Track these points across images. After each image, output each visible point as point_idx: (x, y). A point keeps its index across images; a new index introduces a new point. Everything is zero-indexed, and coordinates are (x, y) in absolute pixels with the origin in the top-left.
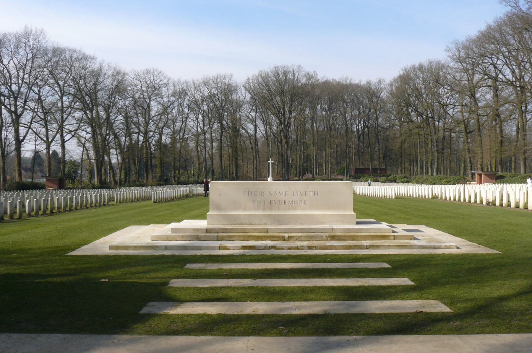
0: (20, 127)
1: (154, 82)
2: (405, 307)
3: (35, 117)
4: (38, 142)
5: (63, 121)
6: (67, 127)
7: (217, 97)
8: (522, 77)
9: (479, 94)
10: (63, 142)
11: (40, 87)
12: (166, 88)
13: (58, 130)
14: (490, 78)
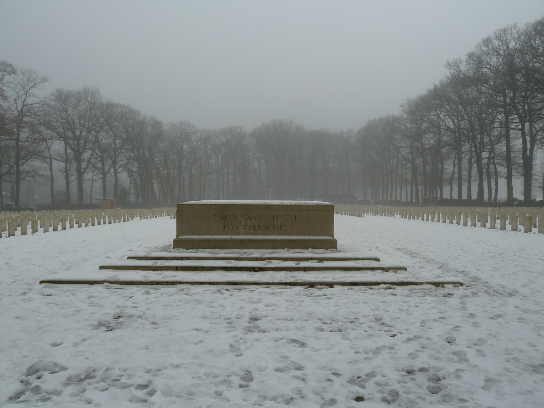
0: (444, 197)
1: (185, 131)
3: (93, 154)
4: (95, 173)
6: (120, 162)
8: (459, 125)
9: (425, 139)
10: (116, 173)
11: (97, 132)
12: (194, 136)
13: (112, 165)
14: (434, 126)
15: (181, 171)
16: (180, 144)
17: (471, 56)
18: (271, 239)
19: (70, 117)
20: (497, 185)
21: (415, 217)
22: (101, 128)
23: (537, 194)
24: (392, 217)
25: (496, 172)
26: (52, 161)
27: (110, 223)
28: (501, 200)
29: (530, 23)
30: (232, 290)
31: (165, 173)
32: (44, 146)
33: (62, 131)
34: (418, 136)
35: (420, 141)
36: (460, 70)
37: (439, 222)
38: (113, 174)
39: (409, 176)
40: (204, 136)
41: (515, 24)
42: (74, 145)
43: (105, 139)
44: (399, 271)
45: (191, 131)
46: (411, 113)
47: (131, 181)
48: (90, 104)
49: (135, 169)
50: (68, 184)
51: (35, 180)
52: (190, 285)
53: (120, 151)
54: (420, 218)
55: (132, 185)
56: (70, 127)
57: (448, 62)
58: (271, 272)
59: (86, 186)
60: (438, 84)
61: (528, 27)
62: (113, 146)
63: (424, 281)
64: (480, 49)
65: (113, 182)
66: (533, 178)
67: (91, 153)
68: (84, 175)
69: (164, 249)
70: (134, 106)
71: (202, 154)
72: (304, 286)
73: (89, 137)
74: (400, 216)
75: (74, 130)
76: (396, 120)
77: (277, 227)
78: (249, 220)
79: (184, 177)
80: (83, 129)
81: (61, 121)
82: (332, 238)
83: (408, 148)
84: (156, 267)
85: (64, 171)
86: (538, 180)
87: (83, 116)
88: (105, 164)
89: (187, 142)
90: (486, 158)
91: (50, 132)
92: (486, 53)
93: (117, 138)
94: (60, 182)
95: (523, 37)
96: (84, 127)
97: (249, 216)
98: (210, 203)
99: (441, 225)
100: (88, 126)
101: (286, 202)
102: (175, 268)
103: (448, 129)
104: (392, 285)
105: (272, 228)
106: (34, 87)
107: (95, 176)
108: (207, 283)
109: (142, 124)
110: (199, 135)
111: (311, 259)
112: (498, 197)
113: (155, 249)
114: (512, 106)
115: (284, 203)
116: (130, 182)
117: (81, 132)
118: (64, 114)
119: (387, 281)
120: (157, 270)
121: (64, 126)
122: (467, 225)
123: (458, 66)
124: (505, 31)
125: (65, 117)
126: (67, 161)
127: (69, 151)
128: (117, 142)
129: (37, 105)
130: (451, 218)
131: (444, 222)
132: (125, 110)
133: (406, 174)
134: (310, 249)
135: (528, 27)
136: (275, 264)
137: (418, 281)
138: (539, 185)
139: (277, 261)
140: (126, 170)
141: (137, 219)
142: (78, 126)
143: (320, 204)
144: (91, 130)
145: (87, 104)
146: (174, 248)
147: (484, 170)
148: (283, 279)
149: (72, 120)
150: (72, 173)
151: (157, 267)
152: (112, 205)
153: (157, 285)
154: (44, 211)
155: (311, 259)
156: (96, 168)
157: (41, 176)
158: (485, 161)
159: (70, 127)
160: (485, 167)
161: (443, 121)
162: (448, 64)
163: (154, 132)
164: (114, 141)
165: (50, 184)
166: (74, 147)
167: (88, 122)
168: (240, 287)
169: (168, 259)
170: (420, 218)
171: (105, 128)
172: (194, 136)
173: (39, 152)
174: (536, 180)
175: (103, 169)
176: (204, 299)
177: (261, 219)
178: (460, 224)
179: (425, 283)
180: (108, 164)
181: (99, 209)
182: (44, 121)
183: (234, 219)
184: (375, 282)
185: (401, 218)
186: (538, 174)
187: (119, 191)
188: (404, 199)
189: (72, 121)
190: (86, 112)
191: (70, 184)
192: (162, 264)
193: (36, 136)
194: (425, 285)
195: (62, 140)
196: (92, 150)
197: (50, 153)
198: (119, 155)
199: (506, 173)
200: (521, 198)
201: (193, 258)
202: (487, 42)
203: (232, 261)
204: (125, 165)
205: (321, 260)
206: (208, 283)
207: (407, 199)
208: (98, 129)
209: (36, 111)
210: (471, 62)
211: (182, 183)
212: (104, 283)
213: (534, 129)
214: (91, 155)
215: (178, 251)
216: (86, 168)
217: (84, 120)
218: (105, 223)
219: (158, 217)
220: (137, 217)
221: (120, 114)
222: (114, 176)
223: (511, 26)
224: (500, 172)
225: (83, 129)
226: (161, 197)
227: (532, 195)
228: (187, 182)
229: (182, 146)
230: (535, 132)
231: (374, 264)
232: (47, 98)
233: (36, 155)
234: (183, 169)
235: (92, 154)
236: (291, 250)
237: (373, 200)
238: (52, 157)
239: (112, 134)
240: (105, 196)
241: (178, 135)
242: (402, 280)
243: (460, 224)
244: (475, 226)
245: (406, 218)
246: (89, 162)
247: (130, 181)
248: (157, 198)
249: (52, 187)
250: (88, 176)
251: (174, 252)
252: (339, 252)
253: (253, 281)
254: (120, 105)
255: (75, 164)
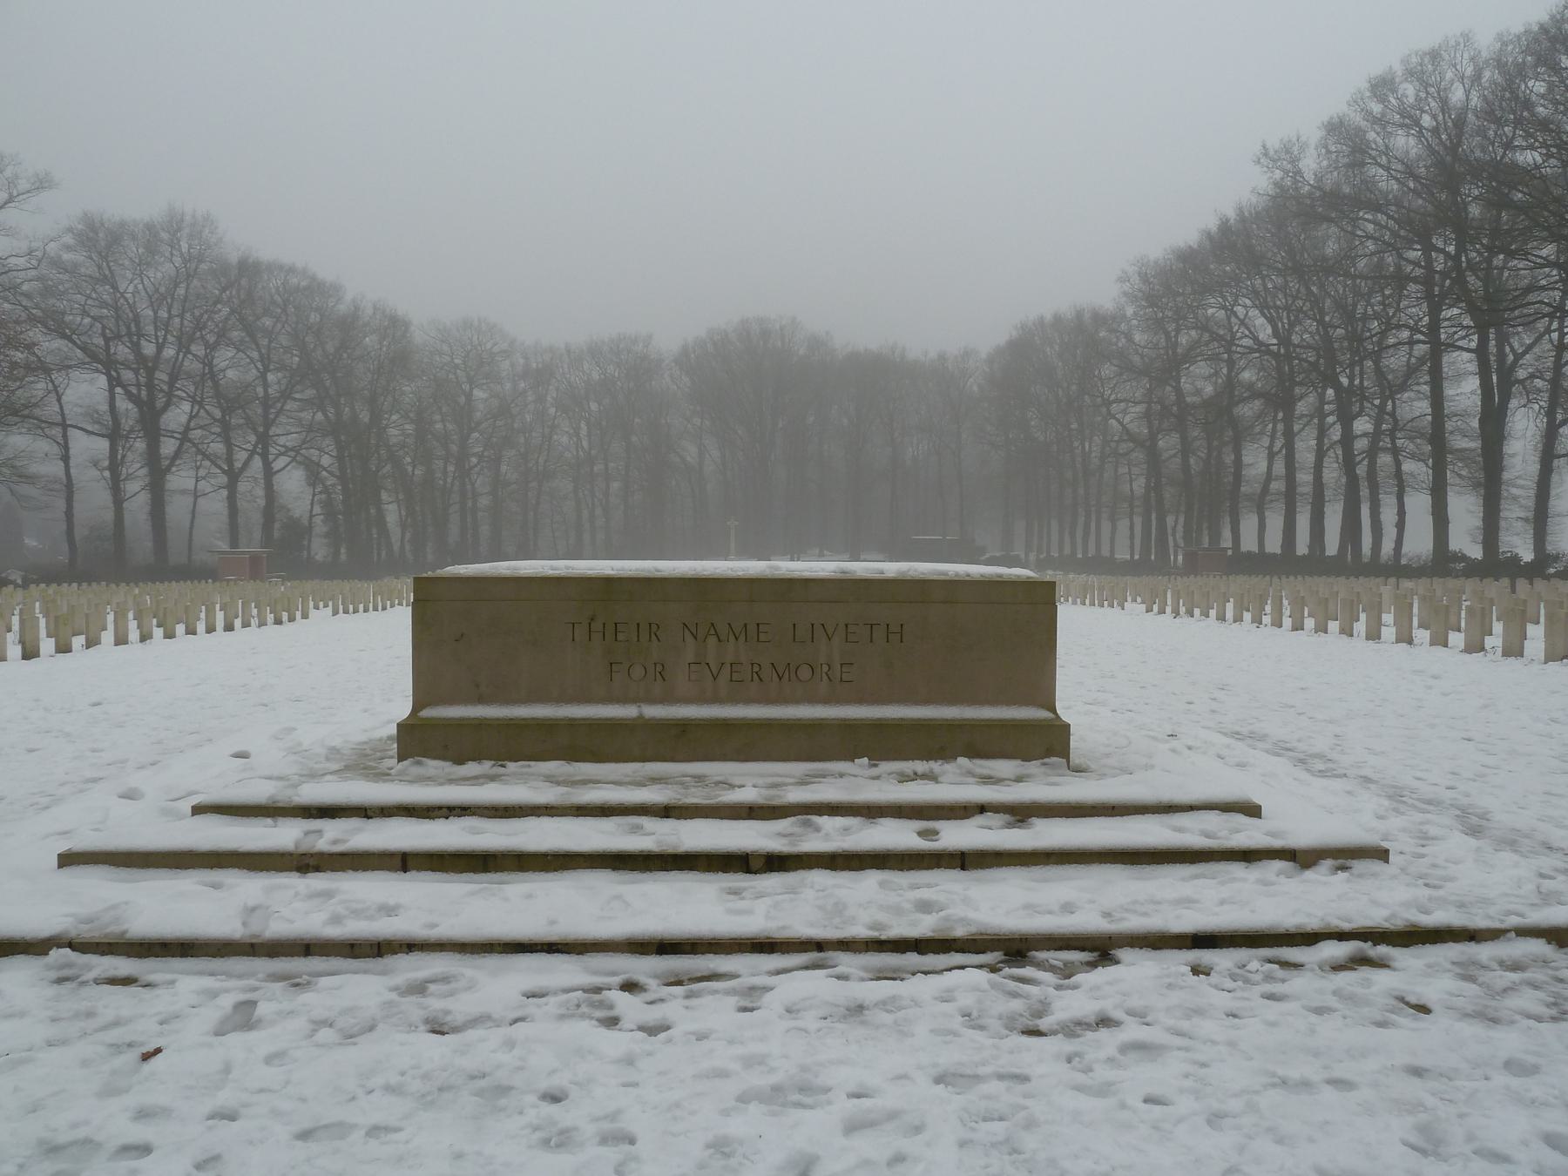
2: (823, 570)
4: (202, 472)
5: (268, 424)
6: (282, 440)
7: (618, 383)
10: (269, 473)
11: (211, 348)
12: (507, 362)
13: (255, 446)
15: (467, 467)
16: (463, 386)
17: (1336, 128)
18: (800, 720)
19: (126, 300)
20: (1401, 513)
21: (1195, 609)
22: (222, 335)
23: (1516, 540)
24: (1117, 609)
25: (1399, 474)
26: (68, 434)
27: (229, 627)
28: (1417, 556)
29: (1510, 34)
30: (655, 989)
31: (420, 472)
32: (40, 387)
33: (101, 342)
34: (1171, 365)
35: (1174, 384)
36: (1299, 172)
37: (1280, 626)
38: (260, 476)
39: (1139, 486)
40: (534, 365)
41: (1467, 35)
42: (138, 385)
43: (233, 367)
44: (1359, 866)
45: (495, 349)
46: (1152, 300)
47: (314, 495)
48: (185, 261)
49: (326, 461)
50: (118, 500)
51: (11, 491)
52: (458, 956)
53: (279, 405)
54: (1213, 613)
55: (317, 509)
56: (123, 331)
57: (1264, 147)
58: (819, 878)
59: (176, 510)
60: (1232, 214)
61: (1505, 44)
62: (260, 390)
63: (1502, 921)
64: (1362, 110)
65: (258, 500)
66: (1505, 494)
67: (189, 411)
68: (168, 477)
69: (362, 763)
70: (325, 272)
71: (528, 418)
72: (983, 952)
73: (183, 361)
74: (1143, 607)
75: (139, 339)
76: (1099, 319)
77: (825, 668)
78: (712, 640)
79: (476, 485)
80: (165, 338)
81: (94, 312)
82: (1043, 714)
83: (1136, 403)
84: (312, 855)
85: (106, 463)
86: (1521, 499)
87: (165, 298)
88: (237, 446)
89: (485, 381)
90: (1365, 435)
91: (59, 343)
92: (1380, 121)
93: (272, 367)
94: (94, 499)
95: (1487, 74)
96: (167, 331)
97: (713, 624)
98: (551, 572)
99: (1307, 638)
100: (181, 329)
101: (862, 568)
102: (398, 862)
103: (1261, 347)
104: (1370, 943)
105: (805, 673)
106: (10, 205)
107: (203, 482)
108: (536, 944)
109: (349, 325)
110: (522, 361)
111: (982, 809)
112: (1405, 549)
113: (328, 759)
114: (1450, 278)
115: (855, 571)
116: (313, 500)
117: (160, 348)
118: (105, 291)
119: (1346, 926)
120: (317, 869)
121: (104, 328)
122: (1379, 638)
123: (1294, 161)
124: (1434, 55)
125: (110, 301)
126: (114, 435)
127: (123, 404)
128: (271, 377)
129: (21, 262)
130: (1252, 607)
131: (1298, 626)
132: (294, 281)
133: (1131, 481)
134: (959, 759)
135: (1505, 44)
136: (833, 835)
137: (1479, 922)
138: (1522, 515)
139: (839, 821)
140: (300, 463)
141: (321, 618)
142: (150, 329)
143: (1001, 576)
144: (192, 340)
145: (178, 261)
146: (401, 758)
147: (1361, 470)
148: (882, 917)
149: (132, 307)
150: (130, 471)
151: (316, 854)
152: (256, 569)
153: (302, 960)
154: (70, 585)
155: (982, 809)
156: (206, 456)
157: (30, 479)
158: (1361, 444)
159: (123, 331)
160: (1363, 459)
161: (1242, 323)
162: (1266, 154)
163: (384, 349)
164: (263, 376)
165: (61, 504)
166: (139, 390)
167: (181, 316)
168: (691, 961)
169: (369, 813)
170: (1213, 613)
171: (235, 335)
172: (507, 362)
173: (26, 407)
174: (1515, 498)
175: (230, 460)
176: (520, 1068)
177: (762, 637)
178: (1352, 636)
179: (1513, 934)
180: (244, 446)
181: (214, 581)
182: (43, 311)
183: (653, 637)
184: (1293, 930)
185: (1147, 612)
186: (1521, 482)
187: (277, 525)
188: (1122, 555)
189: (132, 311)
190: (176, 285)
191: (125, 505)
192: (344, 841)
193: (19, 356)
194: (1509, 940)
195: (97, 371)
196: (194, 401)
197: (61, 408)
198: (277, 417)
199: (1431, 478)
200: (1476, 552)
201: (479, 808)
202: (1382, 87)
203: (648, 823)
204: (296, 450)
205: (1021, 813)
206: (542, 944)
207: (1132, 555)
208: (212, 339)
209: (19, 281)
210: (1333, 148)
211: (470, 504)
212: (54, 953)
213: (1507, 349)
214: (191, 418)
215: (416, 770)
216: (177, 454)
217: (169, 312)
218: (210, 629)
219: (391, 607)
220: (324, 607)
221: (279, 295)
222: (262, 481)
223: (1453, 40)
224: (1412, 475)
225: (165, 338)
226: (407, 547)
227: (1500, 544)
228: (484, 501)
229: (471, 394)
230: (1511, 357)
231: (1247, 834)
232: (52, 241)
233: (15, 413)
234: (474, 460)
235: (194, 414)
236: (886, 767)
237: (1032, 557)
238: (68, 422)
239: (255, 355)
240: (234, 542)
241: (456, 361)
242: (1407, 920)
243: (1352, 636)
244: (1410, 642)
245: (1162, 611)
246: (184, 437)
247: (311, 497)
248: (396, 547)
249: (69, 514)
250: (180, 480)
251: (402, 778)
252: (1079, 770)
253: (749, 936)
254: (281, 267)
255: (140, 445)
